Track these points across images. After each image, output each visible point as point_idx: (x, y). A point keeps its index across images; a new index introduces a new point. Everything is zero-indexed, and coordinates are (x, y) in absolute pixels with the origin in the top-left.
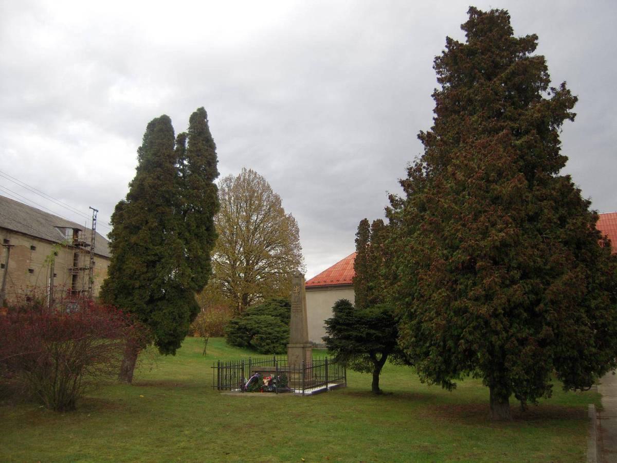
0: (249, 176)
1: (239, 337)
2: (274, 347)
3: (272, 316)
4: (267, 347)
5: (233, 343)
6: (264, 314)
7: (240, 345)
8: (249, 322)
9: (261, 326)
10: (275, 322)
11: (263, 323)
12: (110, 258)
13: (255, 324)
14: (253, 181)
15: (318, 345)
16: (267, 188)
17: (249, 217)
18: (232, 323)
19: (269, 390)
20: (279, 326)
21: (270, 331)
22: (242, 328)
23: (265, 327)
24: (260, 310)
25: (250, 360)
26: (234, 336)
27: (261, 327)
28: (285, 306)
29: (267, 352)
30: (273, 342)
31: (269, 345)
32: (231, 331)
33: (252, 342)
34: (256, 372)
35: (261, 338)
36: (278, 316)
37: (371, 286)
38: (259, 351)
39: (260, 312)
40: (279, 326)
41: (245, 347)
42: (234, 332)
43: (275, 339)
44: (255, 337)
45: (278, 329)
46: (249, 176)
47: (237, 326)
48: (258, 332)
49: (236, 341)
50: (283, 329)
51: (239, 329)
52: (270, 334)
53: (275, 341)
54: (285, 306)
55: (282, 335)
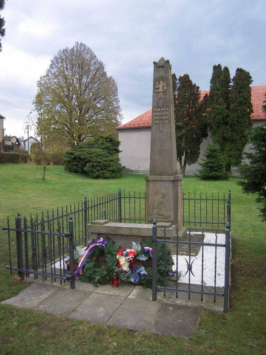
0: (81, 48)
1: (75, 165)
2: (103, 173)
3: (101, 149)
4: (97, 173)
5: (70, 169)
6: (94, 148)
7: (76, 172)
8: (83, 153)
9: (93, 156)
10: (103, 153)
11: (94, 154)
12: (224, 245)
13: (87, 155)
14: (83, 52)
15: (133, 171)
16: (93, 57)
17: (80, 80)
18: (68, 153)
19: (132, 280)
20: (107, 157)
21: (100, 160)
22: (76, 158)
23: (96, 157)
24: (90, 145)
25: (85, 202)
26: (71, 165)
27: (93, 157)
28: (110, 141)
29: (97, 177)
30: (102, 169)
31: (98, 171)
32: (68, 160)
33: (85, 169)
34: (99, 235)
35: (93, 166)
36: (105, 149)
37: (180, 125)
38: (91, 176)
39: (90, 145)
40: (107, 157)
41: (80, 173)
42: (71, 161)
43: (103, 166)
44: (88, 165)
45: (106, 159)
46: (81, 48)
47: (73, 156)
48: (90, 161)
49: (72, 168)
50: (110, 158)
51: (75, 159)
52: (99, 162)
53: (103, 168)
54: (110, 141)
55: (109, 164)
